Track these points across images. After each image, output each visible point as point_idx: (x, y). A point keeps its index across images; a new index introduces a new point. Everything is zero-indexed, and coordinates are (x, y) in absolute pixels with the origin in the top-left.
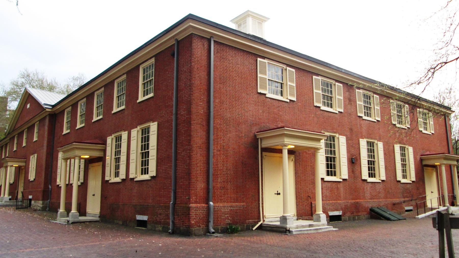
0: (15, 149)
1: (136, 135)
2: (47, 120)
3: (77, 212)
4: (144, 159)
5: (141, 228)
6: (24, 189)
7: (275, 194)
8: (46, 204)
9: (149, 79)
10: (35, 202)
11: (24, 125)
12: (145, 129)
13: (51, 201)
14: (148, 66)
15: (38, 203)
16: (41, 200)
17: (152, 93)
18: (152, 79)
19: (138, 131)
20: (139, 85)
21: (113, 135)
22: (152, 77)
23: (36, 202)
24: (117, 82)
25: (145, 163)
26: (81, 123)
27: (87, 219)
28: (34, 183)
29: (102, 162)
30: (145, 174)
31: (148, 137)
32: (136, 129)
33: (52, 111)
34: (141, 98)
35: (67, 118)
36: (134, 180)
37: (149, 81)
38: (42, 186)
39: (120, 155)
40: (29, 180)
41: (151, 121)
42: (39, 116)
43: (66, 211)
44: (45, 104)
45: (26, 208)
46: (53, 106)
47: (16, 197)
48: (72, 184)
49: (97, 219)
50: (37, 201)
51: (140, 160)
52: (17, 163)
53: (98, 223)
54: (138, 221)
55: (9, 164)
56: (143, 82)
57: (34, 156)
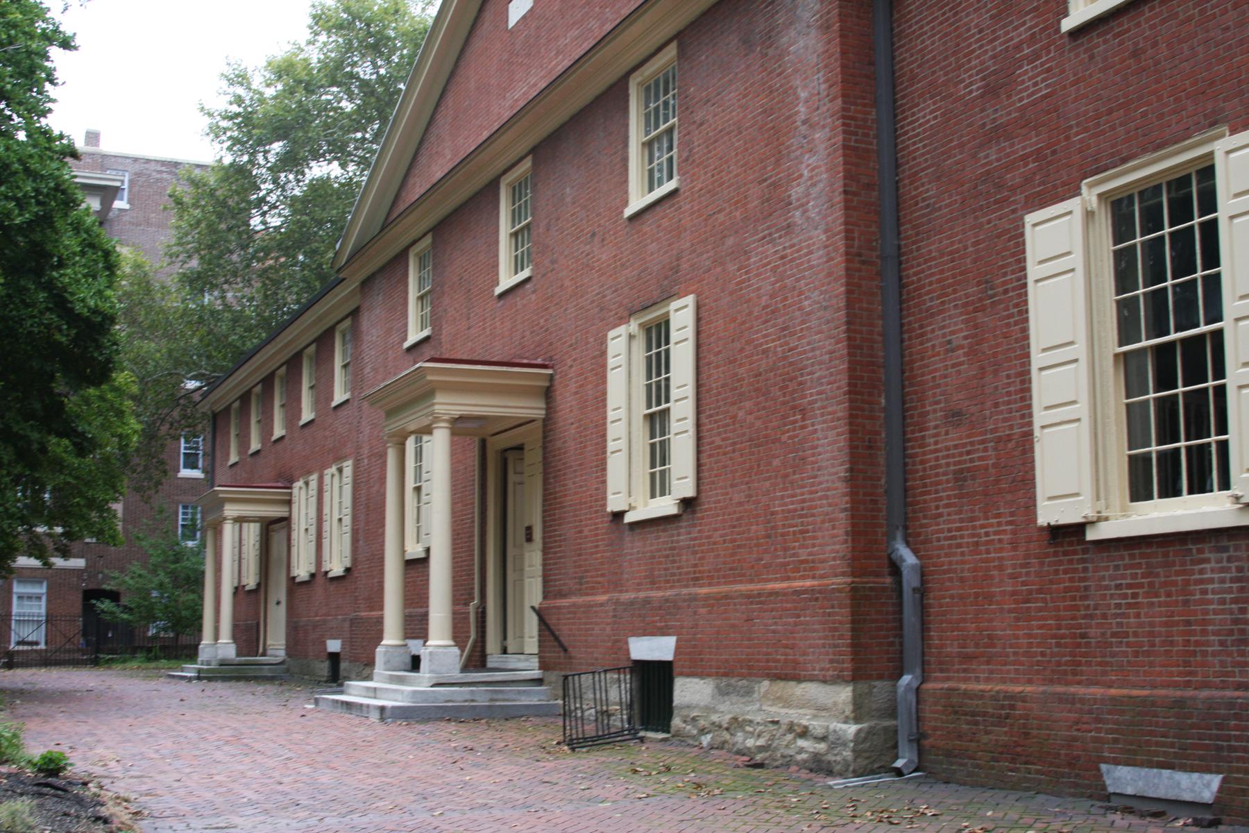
9: (526, 219)
10: (722, 692)
11: (498, 134)
24: (508, 184)
26: (518, 266)
28: (683, 535)
30: (663, 494)
31: (1211, 230)
32: (1074, 204)
35: (420, 286)
36: (1084, 534)
39: (667, 401)
45: (600, 740)
47: (475, 642)
56: (646, 136)
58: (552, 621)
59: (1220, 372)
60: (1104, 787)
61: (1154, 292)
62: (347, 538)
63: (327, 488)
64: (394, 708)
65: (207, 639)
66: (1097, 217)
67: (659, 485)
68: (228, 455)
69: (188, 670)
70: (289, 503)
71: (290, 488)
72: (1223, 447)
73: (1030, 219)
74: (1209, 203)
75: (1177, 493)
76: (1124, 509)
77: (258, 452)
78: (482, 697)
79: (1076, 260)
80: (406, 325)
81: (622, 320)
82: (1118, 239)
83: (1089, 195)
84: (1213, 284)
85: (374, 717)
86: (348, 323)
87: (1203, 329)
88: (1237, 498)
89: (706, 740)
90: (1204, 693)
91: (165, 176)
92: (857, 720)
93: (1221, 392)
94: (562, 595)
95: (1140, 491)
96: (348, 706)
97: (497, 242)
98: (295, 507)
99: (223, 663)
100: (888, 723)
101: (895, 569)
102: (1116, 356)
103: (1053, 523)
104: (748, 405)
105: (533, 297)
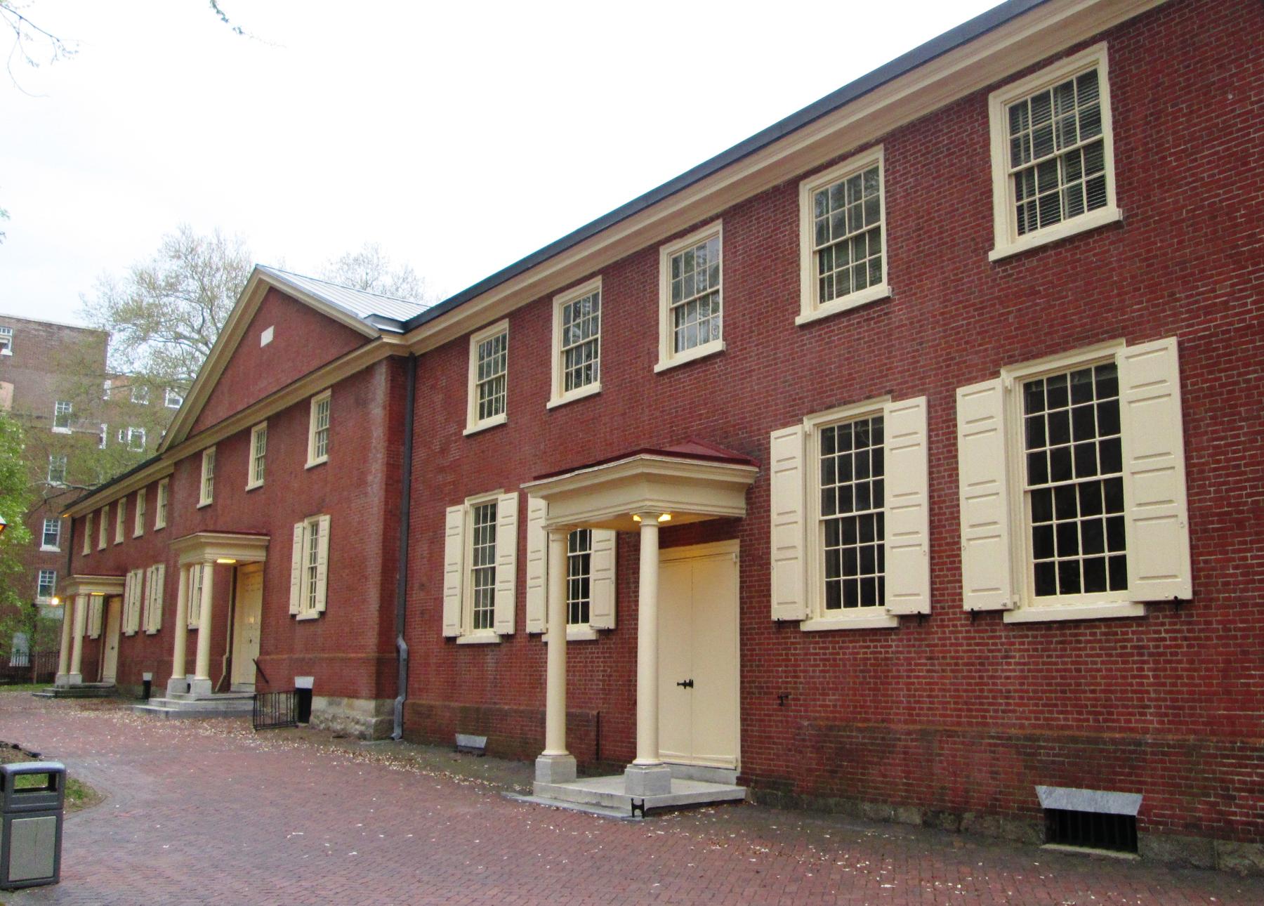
0: (204, 500)
1: (460, 523)
2: (380, 385)
3: (567, 753)
4: (482, 588)
5: (1113, 854)
6: (263, 651)
7: (678, 684)
8: (392, 712)
12: (485, 507)
13: (409, 701)
14: (683, 252)
15: (351, 707)
16: (370, 698)
17: (596, 380)
18: (504, 376)
19: (466, 513)
20: (989, 181)
21: (805, 419)
22: (503, 370)
23: (339, 704)
25: (579, 589)
27: (701, 795)
28: (319, 629)
29: (737, 541)
30: (485, 627)
31: (879, 455)
32: (797, 429)
33: (403, 343)
34: (559, 396)
36: (1002, 618)
37: (496, 378)
38: (371, 640)
40: (294, 616)
41: (500, 488)
42: (339, 368)
43: (571, 753)
44: (375, 315)
45: (279, 725)
46: (408, 327)
47: (225, 677)
48: (536, 636)
49: (733, 790)
50: (345, 701)
51: (470, 589)
52: (101, 588)
53: (740, 809)
54: (1051, 813)
55: (207, 556)
56: (1013, 166)
57: (136, 575)
58: (262, 666)
59: (881, 537)
60: (1039, 804)
61: (829, 489)
62: (159, 612)
63: (148, 579)
64: (175, 712)
65: (61, 671)
66: (1013, 394)
67: (312, 602)
68: (82, 547)
69: (48, 691)
70: (124, 585)
71: (125, 576)
72: (882, 580)
73: (449, 509)
74: (879, 438)
75: (577, 622)
76: (471, 632)
77: (103, 550)
78: (222, 706)
79: (998, 422)
80: (199, 494)
81: (301, 519)
82: (1029, 409)
83: (808, 423)
84: (879, 486)
85: (163, 716)
86: (167, 480)
87: (872, 511)
88: (888, 611)
89: (322, 726)
90: (486, 706)
91: (41, 333)
92: (377, 716)
93: (881, 548)
94: (268, 653)
95: (833, 603)
96: (149, 711)
97: (200, 482)
98: (127, 589)
99: (73, 687)
100: (390, 718)
101: (398, 651)
102: (820, 522)
103: (976, 609)
104: (347, 571)
105: (263, 496)
